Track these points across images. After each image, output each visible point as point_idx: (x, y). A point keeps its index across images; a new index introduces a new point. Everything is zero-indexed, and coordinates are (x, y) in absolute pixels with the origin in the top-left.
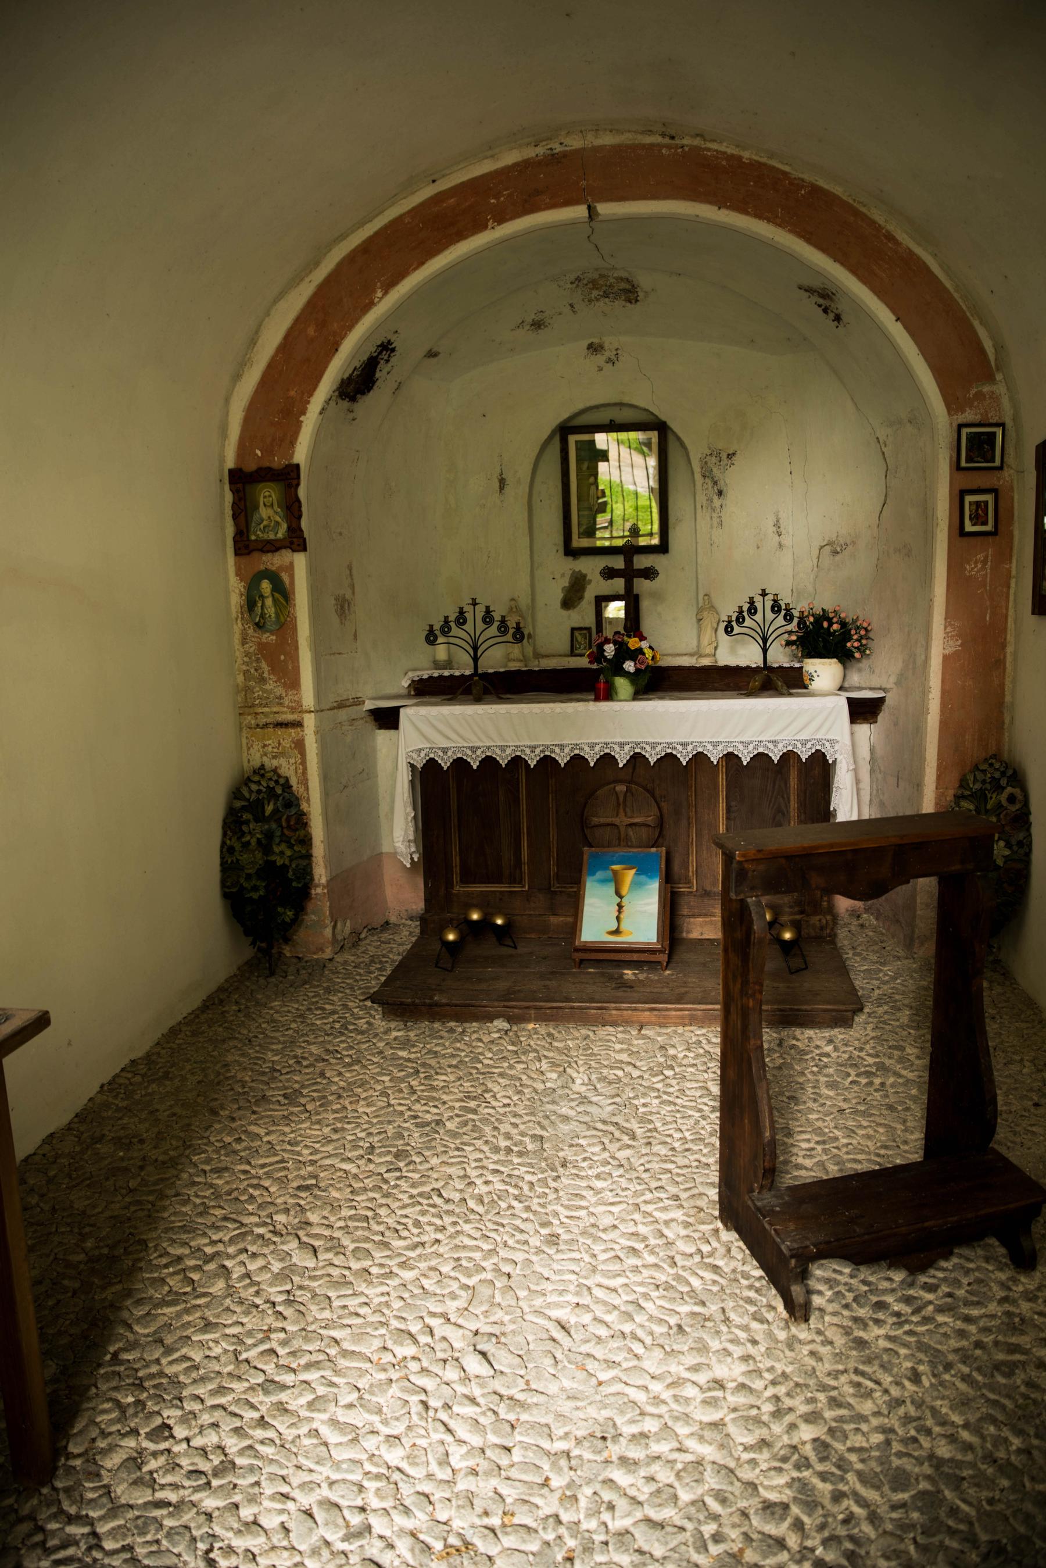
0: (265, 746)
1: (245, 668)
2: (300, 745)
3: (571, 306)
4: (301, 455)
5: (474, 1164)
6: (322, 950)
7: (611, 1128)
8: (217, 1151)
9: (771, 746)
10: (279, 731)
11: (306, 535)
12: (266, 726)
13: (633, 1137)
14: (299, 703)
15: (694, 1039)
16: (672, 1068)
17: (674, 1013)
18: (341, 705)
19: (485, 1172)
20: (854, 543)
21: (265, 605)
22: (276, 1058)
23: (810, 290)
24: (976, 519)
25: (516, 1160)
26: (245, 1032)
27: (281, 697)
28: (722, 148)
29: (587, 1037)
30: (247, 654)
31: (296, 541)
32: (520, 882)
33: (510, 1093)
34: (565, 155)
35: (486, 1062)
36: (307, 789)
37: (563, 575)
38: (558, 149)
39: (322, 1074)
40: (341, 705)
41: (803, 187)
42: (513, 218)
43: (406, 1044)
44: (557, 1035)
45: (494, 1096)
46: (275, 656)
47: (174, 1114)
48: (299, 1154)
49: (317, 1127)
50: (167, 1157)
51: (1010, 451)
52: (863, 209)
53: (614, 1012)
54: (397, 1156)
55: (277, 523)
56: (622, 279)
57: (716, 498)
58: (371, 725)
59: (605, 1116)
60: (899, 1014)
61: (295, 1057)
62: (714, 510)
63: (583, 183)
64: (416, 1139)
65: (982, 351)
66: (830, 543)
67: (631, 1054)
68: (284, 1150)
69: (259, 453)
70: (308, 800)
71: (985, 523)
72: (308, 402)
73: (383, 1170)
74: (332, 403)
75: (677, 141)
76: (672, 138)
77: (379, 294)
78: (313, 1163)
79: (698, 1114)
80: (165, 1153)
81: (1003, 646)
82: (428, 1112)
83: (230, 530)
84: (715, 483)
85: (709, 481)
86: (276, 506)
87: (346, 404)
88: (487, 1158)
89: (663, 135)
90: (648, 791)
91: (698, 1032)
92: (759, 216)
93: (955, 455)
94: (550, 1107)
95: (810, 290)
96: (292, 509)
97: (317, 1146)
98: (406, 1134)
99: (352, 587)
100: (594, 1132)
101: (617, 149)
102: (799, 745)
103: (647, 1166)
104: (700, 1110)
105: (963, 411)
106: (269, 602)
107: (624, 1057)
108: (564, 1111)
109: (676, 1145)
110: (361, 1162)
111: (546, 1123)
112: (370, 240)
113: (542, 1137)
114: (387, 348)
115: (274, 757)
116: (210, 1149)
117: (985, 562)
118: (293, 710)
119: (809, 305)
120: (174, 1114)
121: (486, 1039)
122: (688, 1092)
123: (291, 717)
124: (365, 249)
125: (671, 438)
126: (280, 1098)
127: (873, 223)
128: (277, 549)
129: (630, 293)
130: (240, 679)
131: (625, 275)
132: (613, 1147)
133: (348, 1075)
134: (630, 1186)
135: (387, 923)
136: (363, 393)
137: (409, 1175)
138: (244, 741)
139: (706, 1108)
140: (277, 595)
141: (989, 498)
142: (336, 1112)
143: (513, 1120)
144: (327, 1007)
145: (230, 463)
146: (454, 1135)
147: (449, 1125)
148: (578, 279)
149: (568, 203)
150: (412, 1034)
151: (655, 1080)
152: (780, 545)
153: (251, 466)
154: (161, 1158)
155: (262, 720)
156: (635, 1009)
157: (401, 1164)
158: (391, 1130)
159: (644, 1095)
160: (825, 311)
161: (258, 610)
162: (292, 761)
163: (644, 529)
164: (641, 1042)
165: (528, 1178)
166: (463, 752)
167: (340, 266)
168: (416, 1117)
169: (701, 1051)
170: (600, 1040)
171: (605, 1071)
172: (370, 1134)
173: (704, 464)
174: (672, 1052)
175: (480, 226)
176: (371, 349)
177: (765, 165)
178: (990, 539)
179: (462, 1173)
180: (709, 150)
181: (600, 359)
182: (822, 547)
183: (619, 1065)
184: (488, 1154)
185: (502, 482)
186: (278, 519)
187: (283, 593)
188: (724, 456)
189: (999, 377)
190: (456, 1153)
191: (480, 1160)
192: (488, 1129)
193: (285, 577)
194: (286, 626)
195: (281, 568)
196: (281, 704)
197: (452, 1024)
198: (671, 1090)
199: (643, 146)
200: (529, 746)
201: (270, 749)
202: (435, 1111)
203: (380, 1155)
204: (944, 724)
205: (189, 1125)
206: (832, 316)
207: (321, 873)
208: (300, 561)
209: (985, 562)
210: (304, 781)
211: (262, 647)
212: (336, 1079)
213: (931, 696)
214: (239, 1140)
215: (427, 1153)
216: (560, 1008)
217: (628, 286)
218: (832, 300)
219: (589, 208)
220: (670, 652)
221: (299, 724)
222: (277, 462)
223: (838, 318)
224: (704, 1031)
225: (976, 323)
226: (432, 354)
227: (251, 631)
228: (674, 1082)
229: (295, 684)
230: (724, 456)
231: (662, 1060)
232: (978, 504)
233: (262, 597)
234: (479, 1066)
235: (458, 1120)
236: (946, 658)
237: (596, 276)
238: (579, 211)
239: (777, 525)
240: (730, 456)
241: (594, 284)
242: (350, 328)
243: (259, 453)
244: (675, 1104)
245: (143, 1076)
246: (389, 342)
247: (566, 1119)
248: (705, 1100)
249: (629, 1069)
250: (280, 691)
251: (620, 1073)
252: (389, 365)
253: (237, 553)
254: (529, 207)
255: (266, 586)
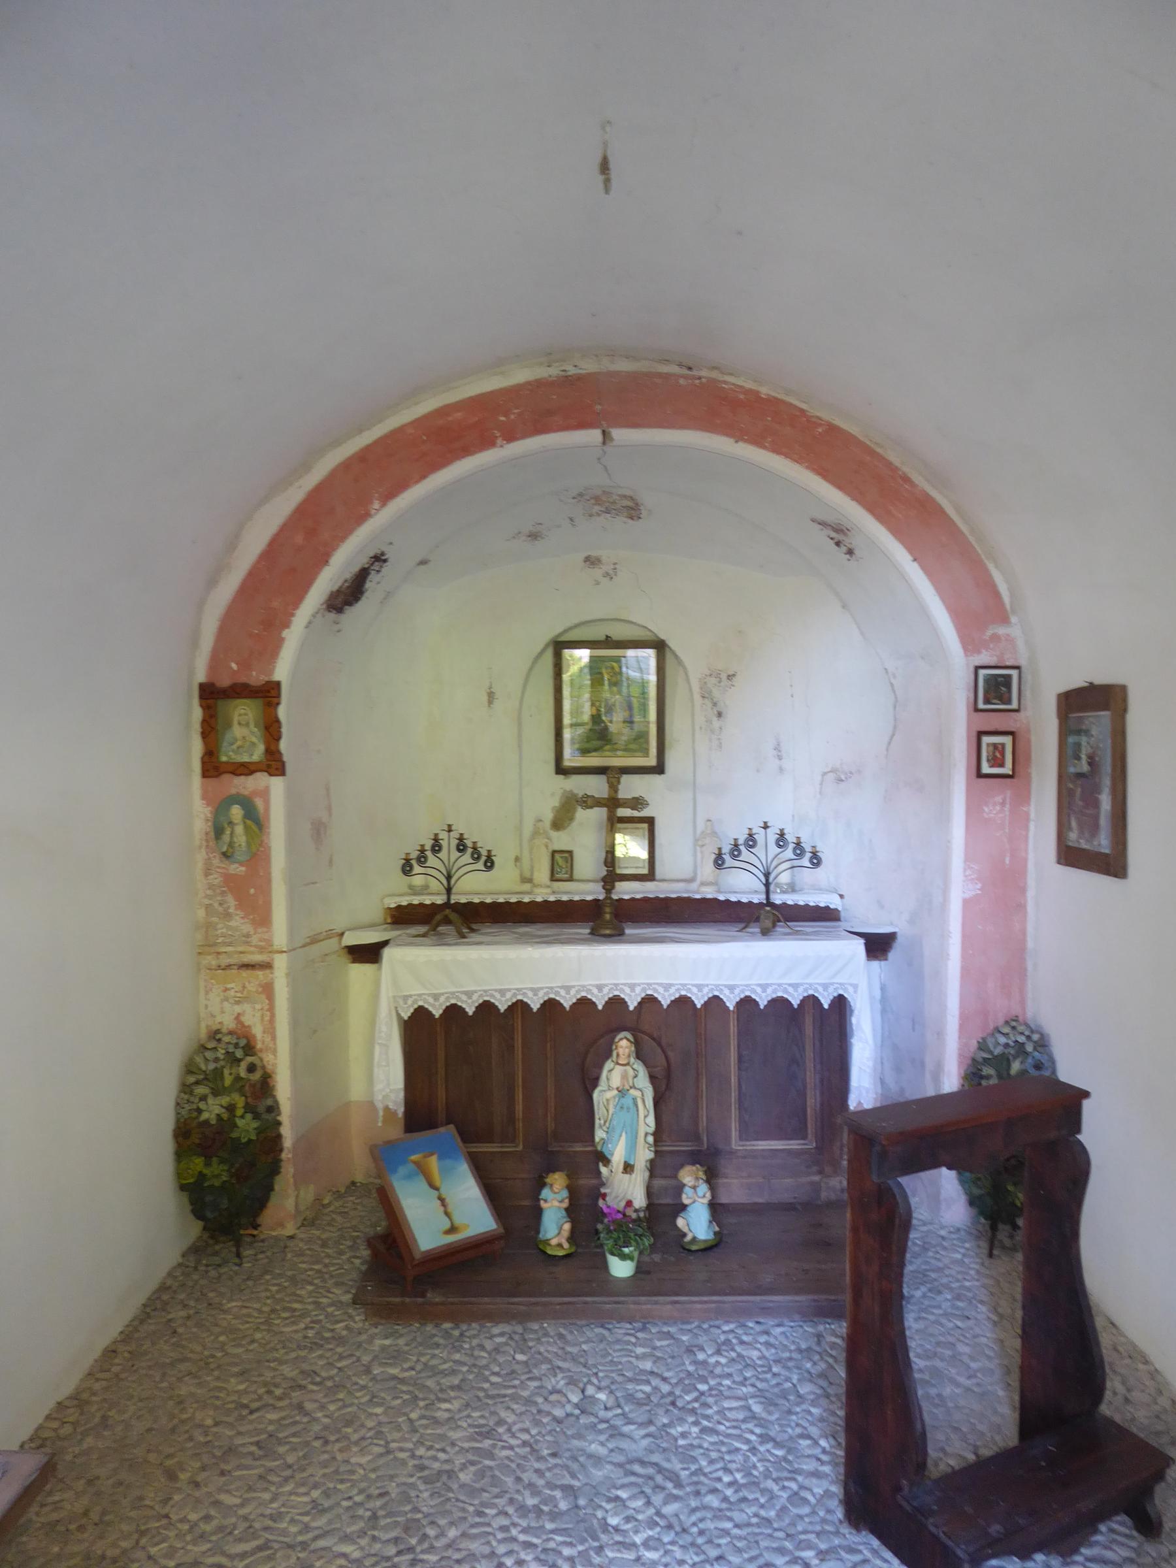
0: (226, 990)
1: (207, 901)
2: (268, 990)
3: (571, 519)
4: (282, 671)
5: (500, 1536)
6: (282, 1225)
7: (651, 1471)
8: (180, 1536)
9: (791, 990)
10: (245, 973)
11: (285, 759)
12: (229, 967)
13: (679, 1485)
14: (269, 942)
15: (723, 1338)
16: (704, 1380)
17: (699, 1306)
18: (314, 941)
19: (516, 1547)
20: (859, 772)
21: (235, 838)
22: (241, 1387)
23: (823, 524)
24: (998, 762)
25: (549, 1526)
26: (199, 1348)
27: (248, 936)
28: (740, 382)
29: (602, 1339)
30: (211, 887)
31: (274, 764)
32: (513, 1141)
33: (527, 1424)
34: (580, 378)
35: (494, 1379)
36: (274, 1038)
37: (553, 795)
38: (572, 371)
39: (300, 1407)
40: (314, 941)
41: (821, 425)
42: (525, 435)
43: (396, 1356)
44: (569, 1337)
45: (509, 1430)
46: (246, 889)
47: (121, 1484)
48: (284, 1533)
49: (302, 1490)
50: (117, 1551)
51: (1027, 693)
52: (878, 450)
53: (632, 1306)
54: (406, 1529)
55: (253, 744)
56: (625, 497)
57: (715, 719)
58: (345, 958)
59: (640, 1454)
60: (939, 1298)
61: (265, 1384)
62: (712, 731)
63: (598, 407)
64: (426, 1500)
65: (997, 595)
66: (833, 771)
67: (657, 1360)
68: (266, 1529)
69: (234, 666)
70: (275, 1052)
71: (1002, 765)
72: (293, 615)
73: (391, 1550)
74: (319, 615)
75: (695, 373)
76: (690, 369)
77: (376, 505)
78: (304, 1545)
79: (745, 1447)
80: (114, 1545)
81: (1023, 890)
82: (435, 1459)
83: (197, 747)
84: (715, 704)
85: (709, 703)
86: (252, 726)
87: (332, 616)
88: (515, 1525)
89: (680, 365)
90: (654, 1039)
91: (726, 1328)
92: (776, 450)
93: (972, 695)
94: (576, 1443)
95: (823, 524)
96: (272, 730)
97: (306, 1519)
98: (413, 1494)
99: (329, 809)
100: (633, 1479)
101: (634, 377)
102: (820, 989)
103: (701, 1526)
104: (748, 1441)
105: (979, 652)
106: (239, 829)
107: (648, 1365)
108: (594, 1448)
109: (729, 1492)
110: (363, 1542)
111: (575, 1466)
112: (368, 449)
113: (571, 1487)
114: (379, 559)
115: (238, 1003)
116: (172, 1534)
117: (1003, 804)
118: (262, 950)
119: (822, 537)
120: (121, 1484)
121: (489, 1345)
122: (728, 1414)
123: (258, 958)
124: (362, 457)
125: (668, 655)
126: (253, 1448)
127: (889, 464)
128: (251, 773)
129: (633, 510)
130: (201, 913)
131: (628, 493)
132: (657, 1499)
133: (332, 1407)
134: (687, 1558)
135: (353, 1183)
136: (350, 604)
137: (425, 1557)
138: (202, 984)
139: (753, 1438)
140: (248, 822)
141: (1007, 740)
142: (324, 1465)
143: (537, 1465)
144: (296, 1306)
145: (201, 676)
146: (473, 1492)
147: (465, 1477)
148: (581, 495)
149: (582, 425)
150: (401, 1342)
151: (688, 1398)
152: (781, 769)
153: (224, 682)
154: (109, 1553)
155: (224, 961)
156: (656, 1303)
157: (413, 1541)
158: (393, 1489)
159: (682, 1420)
160: (838, 544)
161: (226, 837)
162: (258, 1006)
163: (808, 876)
164: (665, 1343)
165: (567, 1551)
166: (458, 998)
167: (333, 474)
168: (422, 1468)
169: (733, 1354)
170: (618, 1341)
171: (630, 1386)
172: (369, 1497)
173: (703, 685)
174: (701, 1356)
175: (487, 442)
176: (363, 561)
177: (783, 402)
178: (1008, 780)
179: (486, 1550)
180: (725, 382)
181: (597, 573)
182: (825, 774)
183: (642, 1377)
184: (516, 1520)
185: (491, 696)
186: (254, 739)
187: (256, 821)
188: (724, 676)
189: (1014, 619)
190: (477, 1520)
191: (504, 1529)
192: (509, 1481)
193: (259, 803)
194: (258, 857)
195: (256, 793)
196: (247, 943)
197: (447, 1325)
198: (709, 1412)
199: (660, 375)
200: (532, 989)
201: (232, 993)
202: (442, 1456)
203: (385, 1528)
204: (965, 971)
205: (141, 1498)
206: (844, 549)
207: (288, 1142)
208: (277, 785)
209: (1003, 804)
210: (271, 1030)
211: (228, 879)
212: (319, 1415)
213: (951, 941)
214: (207, 1518)
215: (442, 1522)
216: (570, 1303)
217: (629, 503)
218: (845, 534)
219: (604, 432)
220: (667, 877)
221: (268, 966)
222: (256, 678)
223: (850, 552)
224: (732, 1326)
225: (991, 567)
226: (423, 562)
227: (216, 862)
228: (710, 1400)
229: (263, 919)
230: (724, 676)
231: (691, 1368)
232: (995, 746)
233: (231, 823)
234: (486, 1386)
235: (472, 1469)
236: (966, 903)
237: (599, 492)
238: (595, 435)
239: (777, 748)
240: (730, 677)
241: (597, 500)
242: (343, 539)
243: (234, 666)
244: (717, 1433)
245: (75, 1424)
246: (383, 554)
247: (597, 1460)
248: (750, 1426)
249: (655, 1382)
250: (247, 928)
251: (647, 1389)
252: (381, 574)
253: (206, 774)
254: (540, 428)
255: (236, 812)
